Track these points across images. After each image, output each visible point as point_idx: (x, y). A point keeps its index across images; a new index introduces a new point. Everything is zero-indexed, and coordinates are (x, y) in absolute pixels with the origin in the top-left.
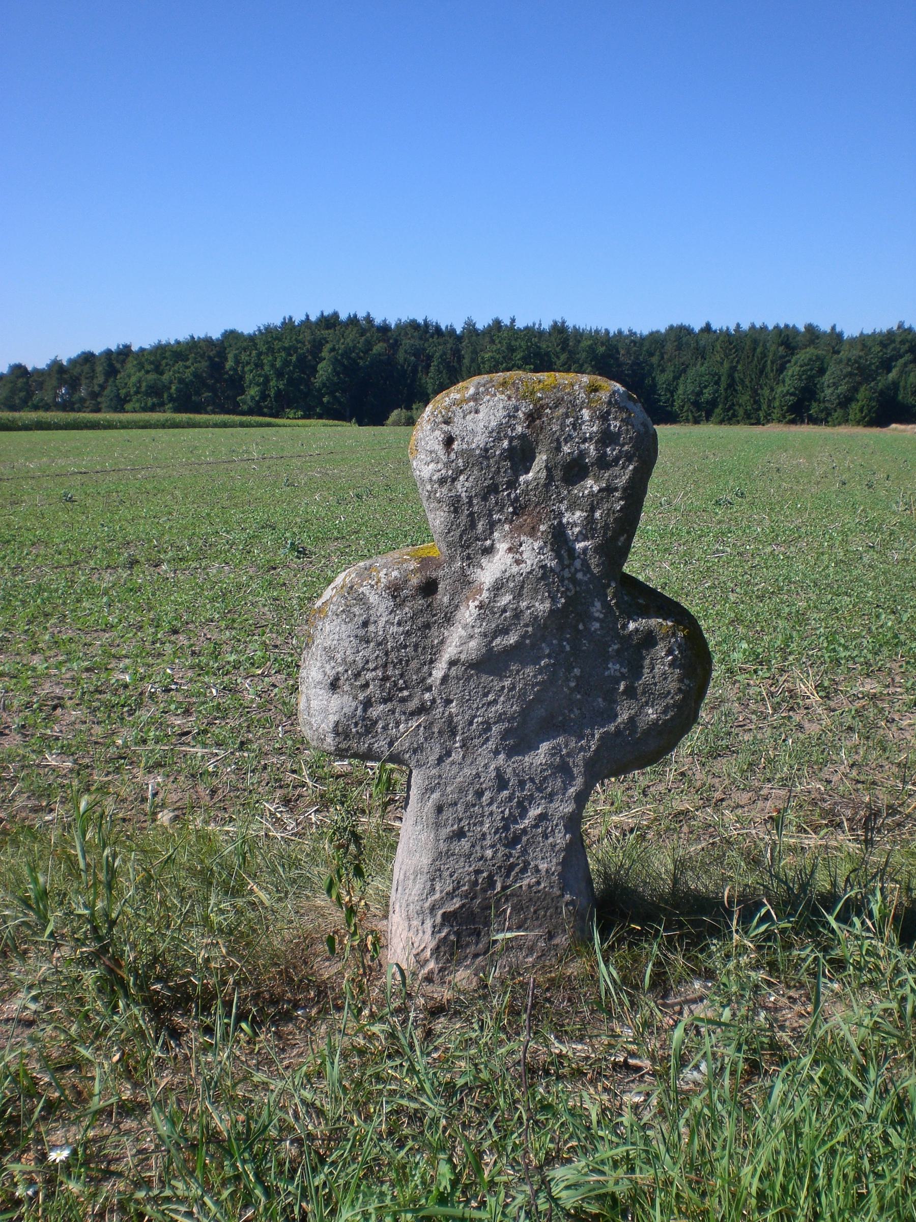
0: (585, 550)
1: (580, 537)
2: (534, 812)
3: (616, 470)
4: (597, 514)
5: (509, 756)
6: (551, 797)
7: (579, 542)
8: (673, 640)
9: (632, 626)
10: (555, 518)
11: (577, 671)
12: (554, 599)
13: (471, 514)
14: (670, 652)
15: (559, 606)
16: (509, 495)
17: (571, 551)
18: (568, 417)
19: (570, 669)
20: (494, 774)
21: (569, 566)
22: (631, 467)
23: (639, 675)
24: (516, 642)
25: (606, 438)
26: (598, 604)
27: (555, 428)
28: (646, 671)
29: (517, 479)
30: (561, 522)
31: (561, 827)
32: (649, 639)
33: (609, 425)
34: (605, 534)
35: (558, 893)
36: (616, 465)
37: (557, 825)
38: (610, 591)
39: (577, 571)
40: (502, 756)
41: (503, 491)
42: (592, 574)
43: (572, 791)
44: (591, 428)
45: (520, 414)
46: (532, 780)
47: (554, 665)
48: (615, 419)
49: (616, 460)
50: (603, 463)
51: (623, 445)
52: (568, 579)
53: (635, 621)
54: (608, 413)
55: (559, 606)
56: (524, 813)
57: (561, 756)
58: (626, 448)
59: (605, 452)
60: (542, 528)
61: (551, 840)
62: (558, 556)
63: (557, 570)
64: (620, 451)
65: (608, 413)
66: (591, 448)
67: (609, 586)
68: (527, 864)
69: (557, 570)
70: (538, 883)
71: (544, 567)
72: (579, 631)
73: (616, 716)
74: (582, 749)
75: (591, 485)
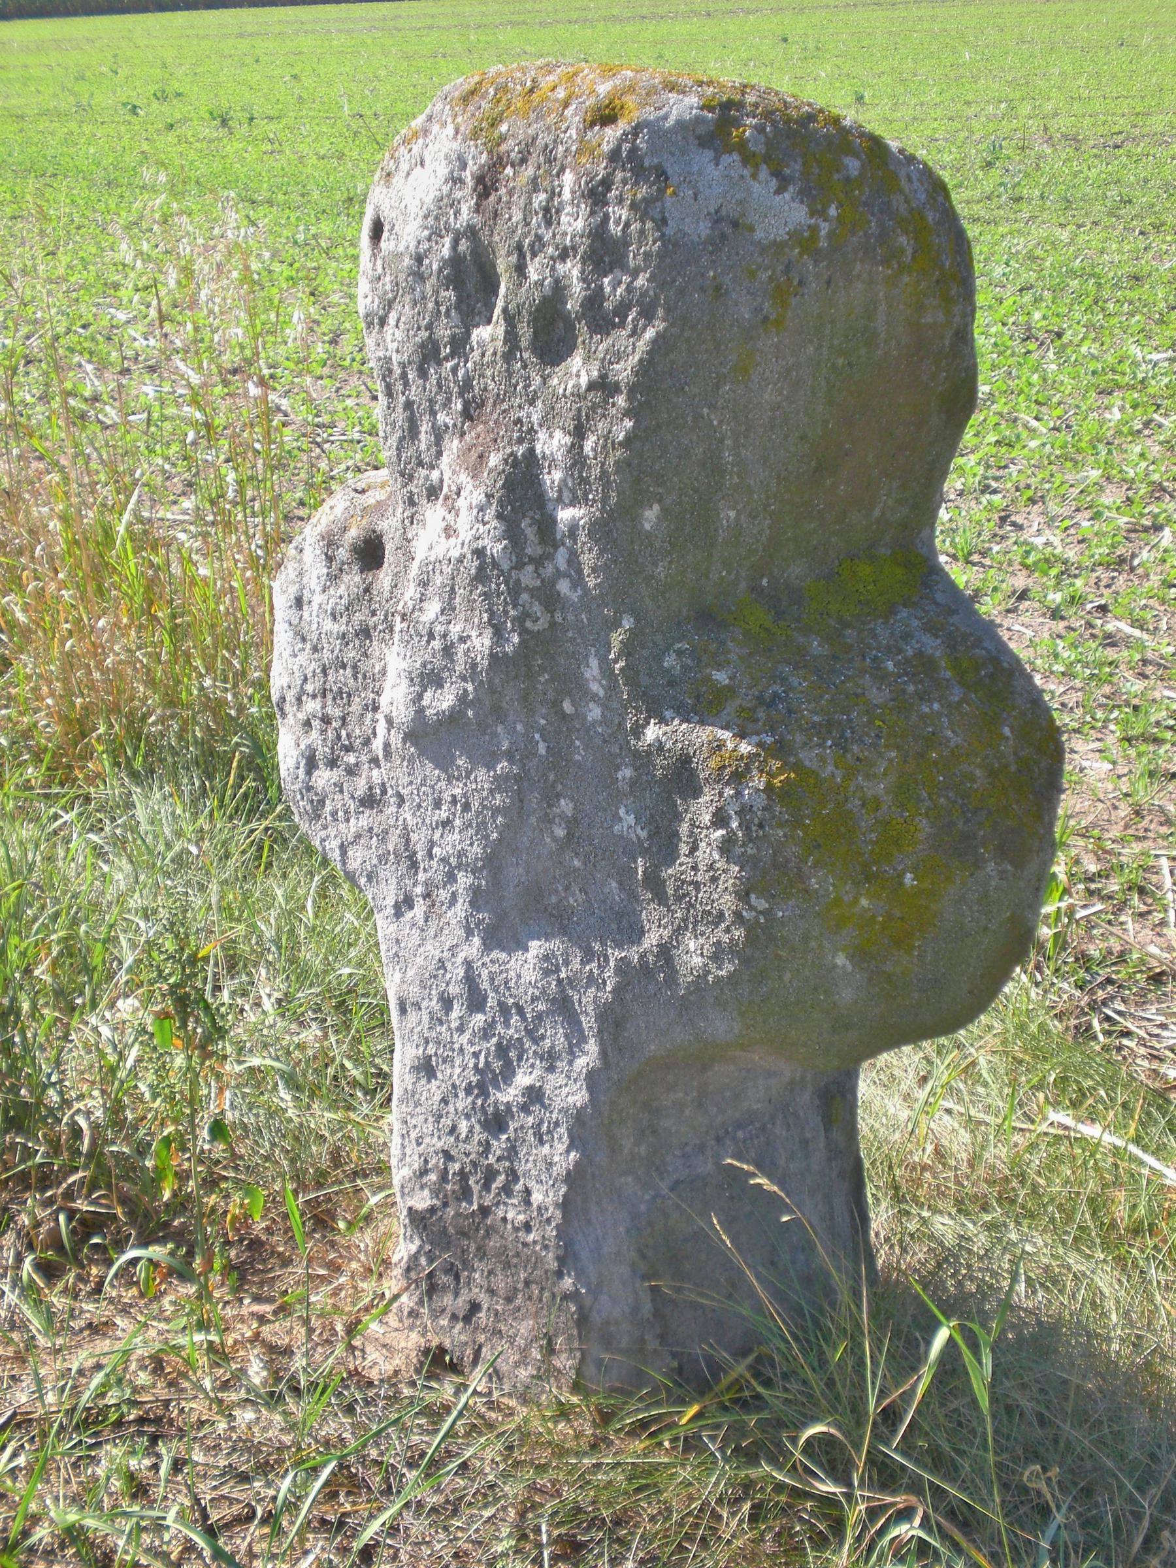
0: (573, 528)
1: (567, 496)
2: (523, 1079)
3: (620, 337)
4: (589, 445)
5: (487, 946)
6: (550, 1060)
7: (566, 506)
8: (729, 792)
9: (652, 733)
10: (520, 441)
11: (565, 806)
12: (498, 633)
13: (409, 405)
14: (720, 819)
15: (509, 649)
16: (454, 370)
17: (547, 526)
18: (536, 190)
19: (550, 797)
20: (461, 972)
21: (539, 562)
22: (650, 334)
23: (671, 857)
24: (452, 707)
25: (603, 252)
26: (594, 662)
27: (517, 216)
28: (684, 849)
29: (468, 334)
30: (532, 450)
31: (562, 1130)
32: (683, 778)
33: (606, 217)
34: (605, 499)
35: (554, 1265)
36: (622, 325)
37: (557, 1124)
38: (617, 639)
39: (559, 574)
40: (476, 941)
41: (446, 359)
42: (586, 591)
43: (581, 1062)
44: (574, 223)
45: (467, 176)
46: (520, 1011)
47: (518, 779)
48: (620, 201)
49: (622, 310)
50: (600, 317)
51: (634, 274)
52: (532, 591)
53: (663, 721)
54: (607, 183)
55: (509, 649)
56: (508, 1073)
57: (560, 982)
58: (641, 281)
59: (601, 288)
60: (494, 460)
61: (546, 1149)
62: (512, 534)
63: (505, 566)
64: (629, 289)
65: (607, 183)
66: (572, 270)
67: (616, 624)
68: (513, 1175)
69: (505, 566)
70: (527, 1227)
71: (479, 553)
72: (564, 716)
73: (642, 932)
74: (591, 980)
75: (578, 370)
